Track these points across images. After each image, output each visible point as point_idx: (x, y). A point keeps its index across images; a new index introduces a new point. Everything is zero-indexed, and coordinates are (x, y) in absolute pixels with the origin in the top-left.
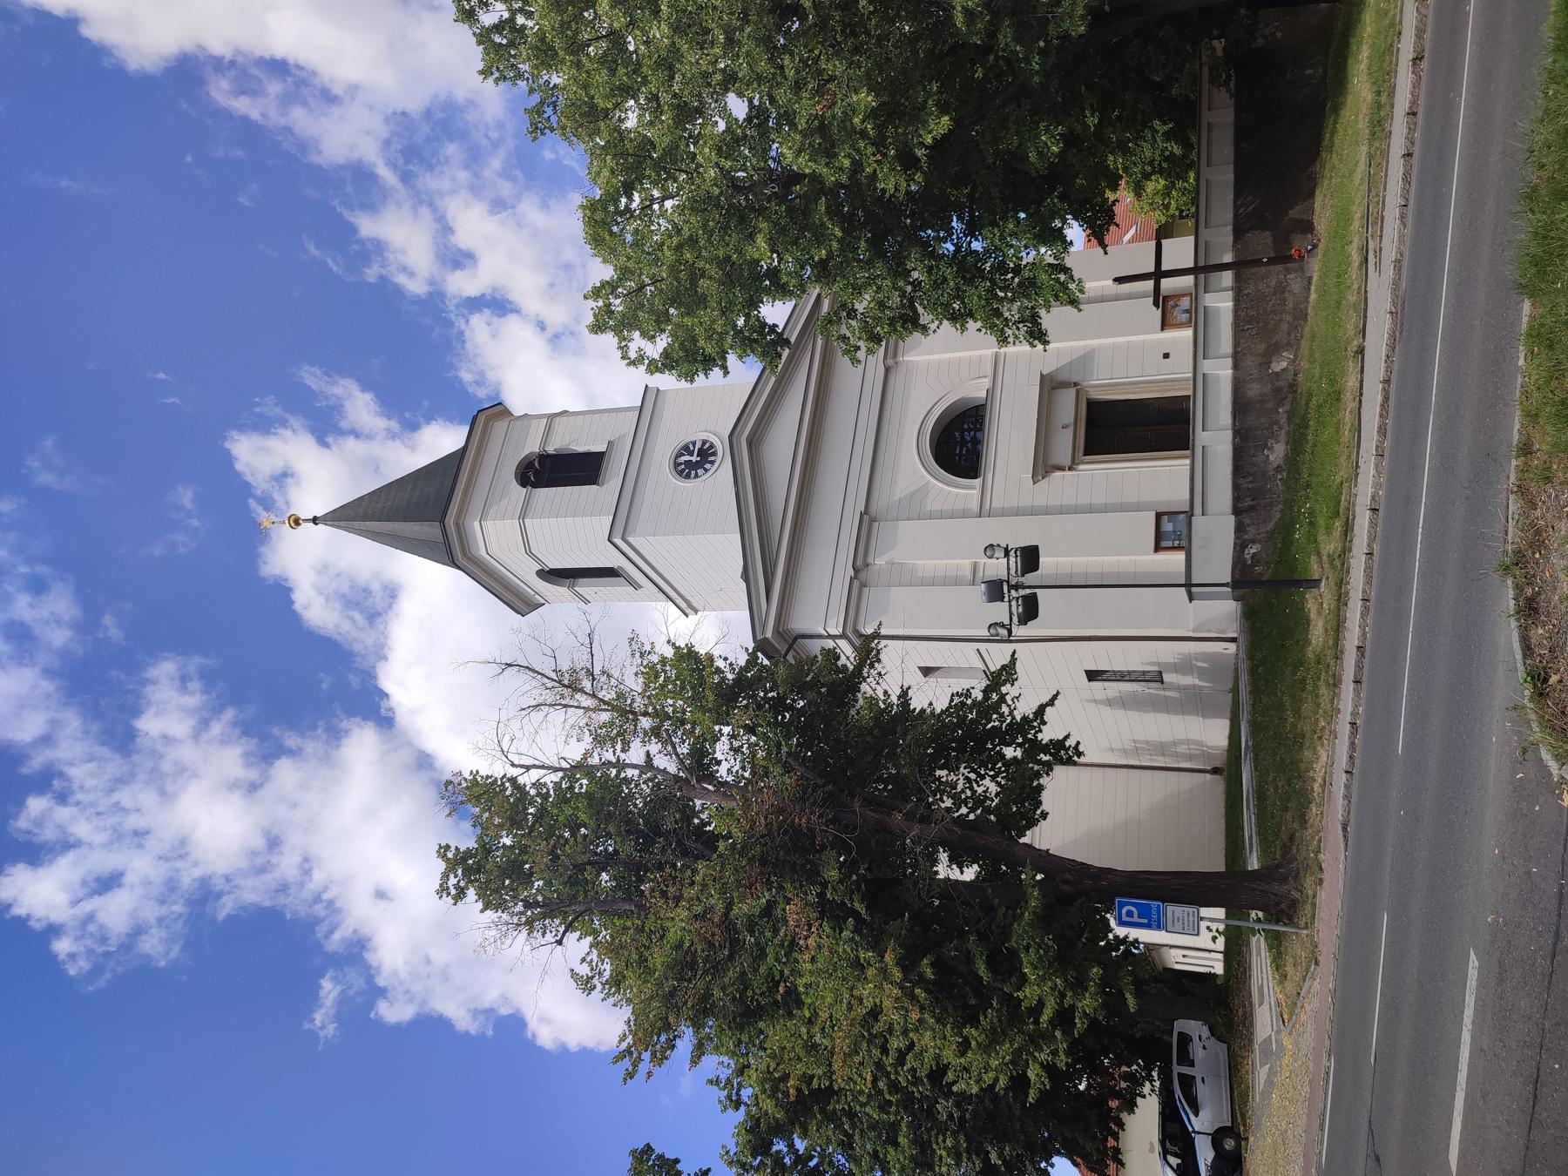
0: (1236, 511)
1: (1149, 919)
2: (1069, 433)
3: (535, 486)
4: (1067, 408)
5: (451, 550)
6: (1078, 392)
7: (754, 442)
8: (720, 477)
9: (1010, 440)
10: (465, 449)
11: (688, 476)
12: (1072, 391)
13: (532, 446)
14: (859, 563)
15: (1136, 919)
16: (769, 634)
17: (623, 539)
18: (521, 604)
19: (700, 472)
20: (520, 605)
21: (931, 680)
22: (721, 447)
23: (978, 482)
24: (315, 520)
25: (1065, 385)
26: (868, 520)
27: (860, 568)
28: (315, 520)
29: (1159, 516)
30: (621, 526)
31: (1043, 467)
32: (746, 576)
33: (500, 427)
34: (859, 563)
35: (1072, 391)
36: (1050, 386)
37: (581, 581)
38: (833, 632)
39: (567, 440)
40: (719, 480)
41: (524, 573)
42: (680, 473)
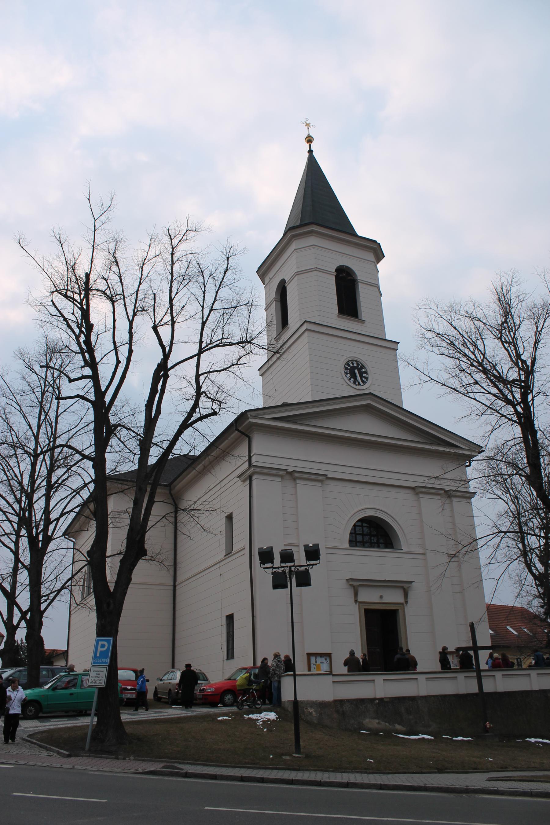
0: (335, 701)
1: (99, 657)
2: (377, 600)
3: (336, 277)
4: (392, 597)
5: (294, 230)
6: (402, 604)
7: (368, 409)
8: (345, 388)
9: (373, 563)
10: (354, 234)
11: (346, 368)
12: (402, 600)
13: (361, 275)
14: (297, 475)
15: (99, 649)
16: (251, 420)
17: (307, 330)
18: (264, 271)
19: (349, 376)
20: (262, 270)
21: (224, 520)
22: (365, 388)
23: (347, 545)
24: (310, 151)
25: (406, 595)
26: (320, 479)
27: (293, 476)
28: (310, 151)
29: (329, 655)
30: (313, 327)
31: (356, 585)
32: (285, 405)
33: (371, 257)
34: (297, 475)
35: (402, 600)
36: (404, 587)
37: (279, 305)
38: (254, 459)
39: (363, 292)
40: (343, 387)
41: (285, 271)
42: (347, 364)
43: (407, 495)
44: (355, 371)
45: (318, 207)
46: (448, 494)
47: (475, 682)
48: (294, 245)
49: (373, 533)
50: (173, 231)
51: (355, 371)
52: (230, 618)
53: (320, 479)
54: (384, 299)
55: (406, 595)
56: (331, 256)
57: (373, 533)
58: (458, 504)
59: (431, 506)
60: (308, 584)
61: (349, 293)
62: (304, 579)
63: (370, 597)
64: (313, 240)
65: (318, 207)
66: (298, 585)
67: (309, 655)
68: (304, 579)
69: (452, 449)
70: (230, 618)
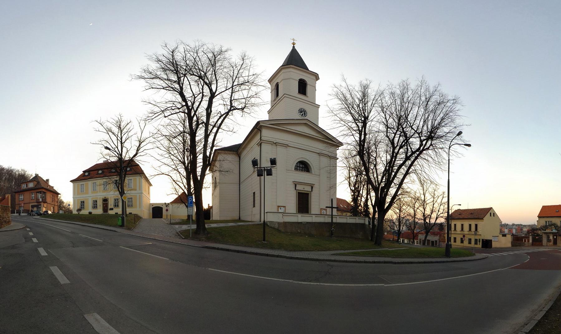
4: (308, 189)
9: (302, 176)
25: (312, 188)
26: (287, 146)
29: (284, 207)
33: (314, 78)
39: (309, 89)
40: (298, 116)
43: (317, 156)
44: (303, 112)
45: (294, 60)
46: (330, 157)
47: (330, 219)
48: (283, 71)
49: (304, 166)
50: (166, 97)
51: (303, 112)
52: (254, 193)
53: (287, 146)
54: (316, 92)
55: (312, 188)
56: (296, 74)
57: (304, 166)
58: (332, 160)
59: (325, 160)
60: (271, 175)
61: (303, 87)
62: (269, 173)
63: (299, 187)
64: (291, 70)
65: (294, 60)
66: (267, 175)
67: (278, 206)
68: (269, 173)
69: (334, 143)
70: (254, 193)
